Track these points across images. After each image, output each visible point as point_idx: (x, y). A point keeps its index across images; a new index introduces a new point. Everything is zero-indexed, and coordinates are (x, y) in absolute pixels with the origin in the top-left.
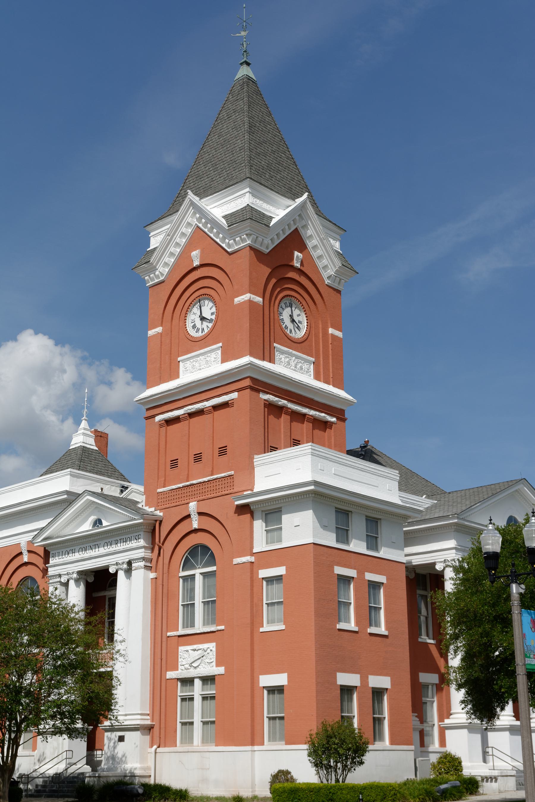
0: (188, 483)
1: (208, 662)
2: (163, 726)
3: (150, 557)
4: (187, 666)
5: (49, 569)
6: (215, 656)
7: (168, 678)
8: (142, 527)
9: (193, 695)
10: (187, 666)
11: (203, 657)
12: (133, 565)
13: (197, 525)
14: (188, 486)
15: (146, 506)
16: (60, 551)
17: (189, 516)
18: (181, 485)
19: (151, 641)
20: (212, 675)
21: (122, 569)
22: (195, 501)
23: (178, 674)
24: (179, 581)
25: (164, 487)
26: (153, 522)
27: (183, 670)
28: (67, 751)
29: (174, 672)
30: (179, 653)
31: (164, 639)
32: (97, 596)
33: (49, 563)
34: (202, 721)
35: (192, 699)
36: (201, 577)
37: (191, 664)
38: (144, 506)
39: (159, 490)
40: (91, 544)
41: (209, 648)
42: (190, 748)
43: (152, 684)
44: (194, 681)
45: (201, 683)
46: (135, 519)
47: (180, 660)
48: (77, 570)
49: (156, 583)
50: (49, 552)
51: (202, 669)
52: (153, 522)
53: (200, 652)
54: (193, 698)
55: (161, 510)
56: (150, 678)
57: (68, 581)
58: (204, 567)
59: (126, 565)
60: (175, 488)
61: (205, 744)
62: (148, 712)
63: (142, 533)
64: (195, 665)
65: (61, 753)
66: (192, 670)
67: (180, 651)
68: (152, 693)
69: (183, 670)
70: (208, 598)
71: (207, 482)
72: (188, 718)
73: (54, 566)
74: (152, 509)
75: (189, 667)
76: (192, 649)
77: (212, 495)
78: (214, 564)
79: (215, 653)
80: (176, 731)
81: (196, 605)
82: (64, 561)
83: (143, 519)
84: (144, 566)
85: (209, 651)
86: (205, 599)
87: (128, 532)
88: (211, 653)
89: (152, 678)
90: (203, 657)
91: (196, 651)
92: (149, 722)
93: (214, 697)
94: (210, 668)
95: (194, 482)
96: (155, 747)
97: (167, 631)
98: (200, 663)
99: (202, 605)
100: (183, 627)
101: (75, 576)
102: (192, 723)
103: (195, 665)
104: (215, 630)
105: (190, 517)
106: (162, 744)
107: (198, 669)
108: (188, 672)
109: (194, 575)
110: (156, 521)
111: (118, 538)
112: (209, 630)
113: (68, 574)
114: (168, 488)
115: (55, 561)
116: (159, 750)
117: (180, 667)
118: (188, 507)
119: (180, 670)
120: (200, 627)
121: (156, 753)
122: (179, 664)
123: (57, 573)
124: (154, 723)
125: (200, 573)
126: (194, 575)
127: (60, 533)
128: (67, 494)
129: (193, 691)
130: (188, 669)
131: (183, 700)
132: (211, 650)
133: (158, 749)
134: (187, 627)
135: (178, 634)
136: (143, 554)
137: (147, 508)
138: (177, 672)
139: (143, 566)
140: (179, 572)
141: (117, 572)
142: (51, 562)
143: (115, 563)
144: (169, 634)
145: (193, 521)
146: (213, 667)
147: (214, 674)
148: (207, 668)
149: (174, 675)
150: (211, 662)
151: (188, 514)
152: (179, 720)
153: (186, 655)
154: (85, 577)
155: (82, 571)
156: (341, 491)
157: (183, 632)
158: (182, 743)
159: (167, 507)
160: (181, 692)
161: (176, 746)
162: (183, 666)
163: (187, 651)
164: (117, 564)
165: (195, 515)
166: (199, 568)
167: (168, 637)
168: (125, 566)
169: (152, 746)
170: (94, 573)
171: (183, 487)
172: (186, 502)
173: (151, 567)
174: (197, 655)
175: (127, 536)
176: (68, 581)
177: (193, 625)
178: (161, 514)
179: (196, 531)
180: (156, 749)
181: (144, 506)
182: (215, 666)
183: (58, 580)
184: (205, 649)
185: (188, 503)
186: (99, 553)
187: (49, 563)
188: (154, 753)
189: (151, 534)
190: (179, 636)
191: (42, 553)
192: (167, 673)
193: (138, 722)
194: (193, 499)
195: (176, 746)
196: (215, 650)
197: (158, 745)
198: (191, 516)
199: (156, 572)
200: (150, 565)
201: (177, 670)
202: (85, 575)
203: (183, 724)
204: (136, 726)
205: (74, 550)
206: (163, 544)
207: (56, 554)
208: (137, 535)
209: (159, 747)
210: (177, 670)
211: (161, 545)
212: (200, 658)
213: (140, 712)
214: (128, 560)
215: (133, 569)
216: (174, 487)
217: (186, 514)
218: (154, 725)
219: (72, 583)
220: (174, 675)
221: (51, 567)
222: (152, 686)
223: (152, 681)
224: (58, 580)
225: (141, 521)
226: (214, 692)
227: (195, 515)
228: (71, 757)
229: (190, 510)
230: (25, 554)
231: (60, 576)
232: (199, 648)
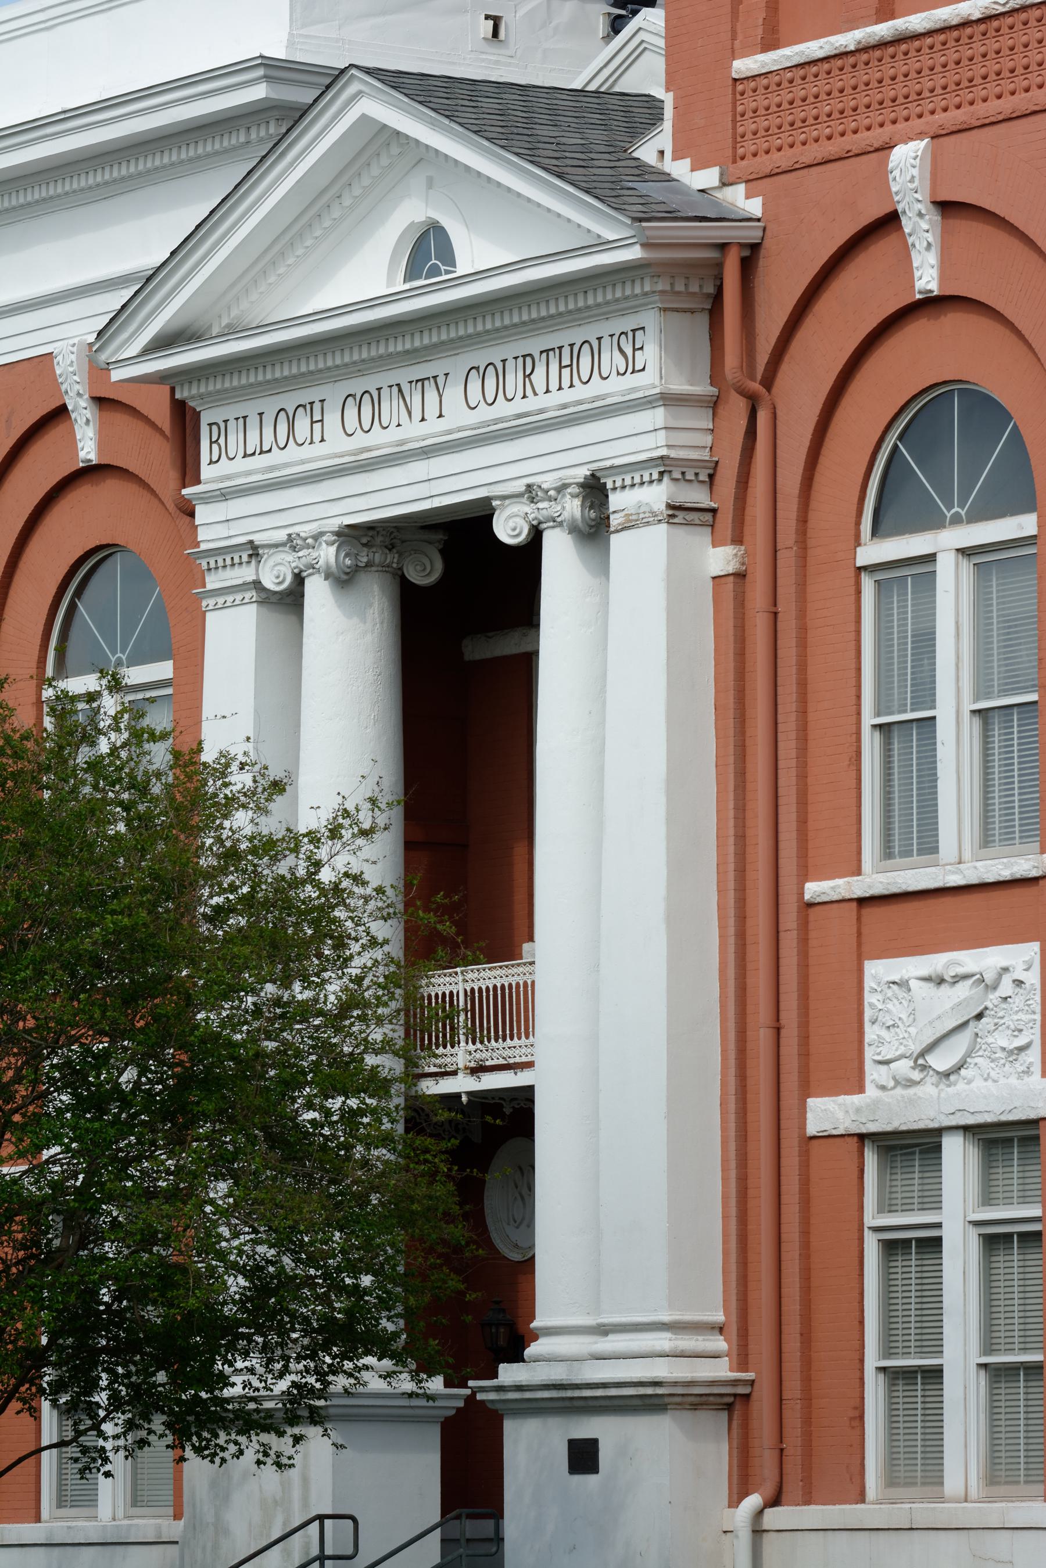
0: (883, 30)
1: (1003, 1049)
2: (793, 1387)
3: (705, 455)
4: (903, 1067)
5: (203, 514)
6: (1038, 1017)
7: (812, 1129)
8: (647, 288)
9: (938, 1226)
10: (903, 1067)
11: (979, 1016)
12: (616, 501)
13: (934, 273)
14: (882, 44)
15: (675, 158)
16: (251, 409)
17: (891, 220)
18: (848, 40)
19: (722, 927)
20: (1022, 1116)
21: (556, 522)
22: (920, 135)
23: (858, 1110)
24: (859, 592)
25: (770, 44)
26: (713, 254)
27: (883, 1088)
28: (321, 1518)
29: (842, 1099)
30: (869, 998)
31: (789, 919)
32: (488, 655)
33: (198, 481)
34: (984, 1366)
35: (933, 1245)
36: (966, 567)
37: (922, 1054)
38: (668, 155)
39: (745, 65)
40: (403, 376)
41: (1006, 970)
42: (923, 1512)
43: (733, 1164)
44: (938, 1148)
45: (974, 1153)
46: (603, 245)
47: (871, 1033)
48: (335, 524)
49: (740, 602)
50: (197, 415)
51: (978, 1083)
52: (713, 254)
53: (963, 990)
54: (938, 1241)
55: (753, 182)
56: (724, 1129)
57: (299, 580)
58: (979, 515)
59: (577, 502)
60: (820, 54)
61: (1002, 1490)
62: (720, 1317)
63: (650, 319)
64: (940, 1061)
65: (297, 1523)
66: (929, 1089)
67: (869, 983)
68: (733, 1211)
69: (883, 1088)
70: (1005, 692)
71: (980, 21)
72: (922, 1354)
73: (224, 495)
74: (708, 178)
75: (916, 1075)
76: (924, 972)
77: (1007, 105)
78: (1026, 505)
79: (1038, 998)
80: (861, 1417)
81: (945, 731)
82: (272, 469)
83: (645, 246)
84: (669, 506)
85: (1006, 987)
86: (988, 696)
87: (579, 310)
88: (1017, 1002)
89: (732, 1133)
90: (979, 1016)
91: (944, 987)
92: (722, 1370)
93: (1038, 1234)
94: (1013, 1081)
95: (916, 22)
96: (753, 1501)
97: (805, 875)
98: (969, 1054)
99: (972, 728)
100: (887, 853)
101: (327, 554)
102: (935, 1374)
103: (940, 1061)
104: (1034, 873)
105: (900, 227)
106: (793, 1486)
107: (961, 1085)
108: (912, 1102)
109: (930, 558)
110: (723, 247)
111: (534, 345)
112: (1006, 874)
113: (291, 543)
114: (787, 51)
115: (225, 467)
116: (774, 1518)
117: (873, 1074)
118: (883, 173)
119: (871, 1091)
120: (967, 855)
121: (758, 1532)
122: (869, 1054)
123: (238, 534)
124: (750, 1375)
125: (962, 551)
126: (930, 558)
127: (244, 305)
128: (267, 78)
129: (936, 1205)
130: (911, 1083)
131: (892, 1248)
132: (1019, 983)
133: (769, 1512)
134: (907, 853)
135: (859, 892)
136: (661, 438)
137: (680, 169)
138: (855, 1099)
139: (660, 506)
140: (858, 543)
141: (536, 535)
142: (207, 472)
143: (519, 486)
144: (813, 889)
145: (914, 254)
146: (1027, 1072)
147: (1033, 1115)
148: (1003, 1081)
149: (840, 1115)
150: (1021, 1049)
151: (888, 209)
152: (872, 1360)
153: (898, 1010)
154: (392, 558)
155: (370, 528)
156: (680, 463)
157: (882, 878)
158: (891, 1480)
159: (785, 165)
160: (886, 1206)
161: (861, 1498)
162: (883, 1068)
163: (903, 984)
164: (531, 493)
165: (920, 215)
166: (956, 520)
167: (810, 905)
168: (572, 507)
169: (735, 1500)
170: (440, 536)
171: (863, 49)
172: (876, 137)
173: (714, 511)
174: (948, 1005)
175: (576, 336)
176: (299, 580)
177: (929, 846)
178: (754, 207)
179: (931, 304)
180: (760, 1513)
181: (668, 155)
182: (1037, 1069)
183: (246, 574)
184: (989, 977)
185: (888, 147)
186: (442, 425)
187: (198, 481)
188: (744, 1536)
189: (702, 322)
190: (862, 902)
191: (162, 416)
192: (811, 1102)
193: (660, 1370)
194: (916, 124)
195: (861, 1498)
196: (1038, 986)
197: (770, 1488)
198: (904, 221)
199: (738, 539)
200: (705, 502)
201: (861, 1089)
202: (391, 548)
203: (893, 1376)
204: (649, 1391)
205: (317, 407)
206: (768, 382)
207: (232, 424)
208: (628, 328)
209: (775, 1501)
210: (861, 1089)
211: (756, 386)
212: (964, 1025)
213: (665, 1317)
214: (583, 472)
215: (615, 521)
216: (815, 48)
217: (876, 211)
218: (752, 1383)
219: (317, 590)
220: (840, 1115)
221: (208, 498)
222: (733, 1174)
223: (732, 1146)
224: (246, 574)
225: (634, 253)
226: (1036, 1211)
227: (920, 215)
228: (350, 1551)
229: (894, 189)
230: (81, 421)
231: (254, 551)
232: (961, 970)
